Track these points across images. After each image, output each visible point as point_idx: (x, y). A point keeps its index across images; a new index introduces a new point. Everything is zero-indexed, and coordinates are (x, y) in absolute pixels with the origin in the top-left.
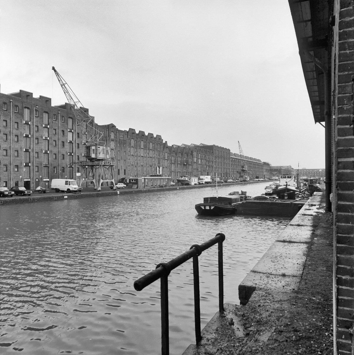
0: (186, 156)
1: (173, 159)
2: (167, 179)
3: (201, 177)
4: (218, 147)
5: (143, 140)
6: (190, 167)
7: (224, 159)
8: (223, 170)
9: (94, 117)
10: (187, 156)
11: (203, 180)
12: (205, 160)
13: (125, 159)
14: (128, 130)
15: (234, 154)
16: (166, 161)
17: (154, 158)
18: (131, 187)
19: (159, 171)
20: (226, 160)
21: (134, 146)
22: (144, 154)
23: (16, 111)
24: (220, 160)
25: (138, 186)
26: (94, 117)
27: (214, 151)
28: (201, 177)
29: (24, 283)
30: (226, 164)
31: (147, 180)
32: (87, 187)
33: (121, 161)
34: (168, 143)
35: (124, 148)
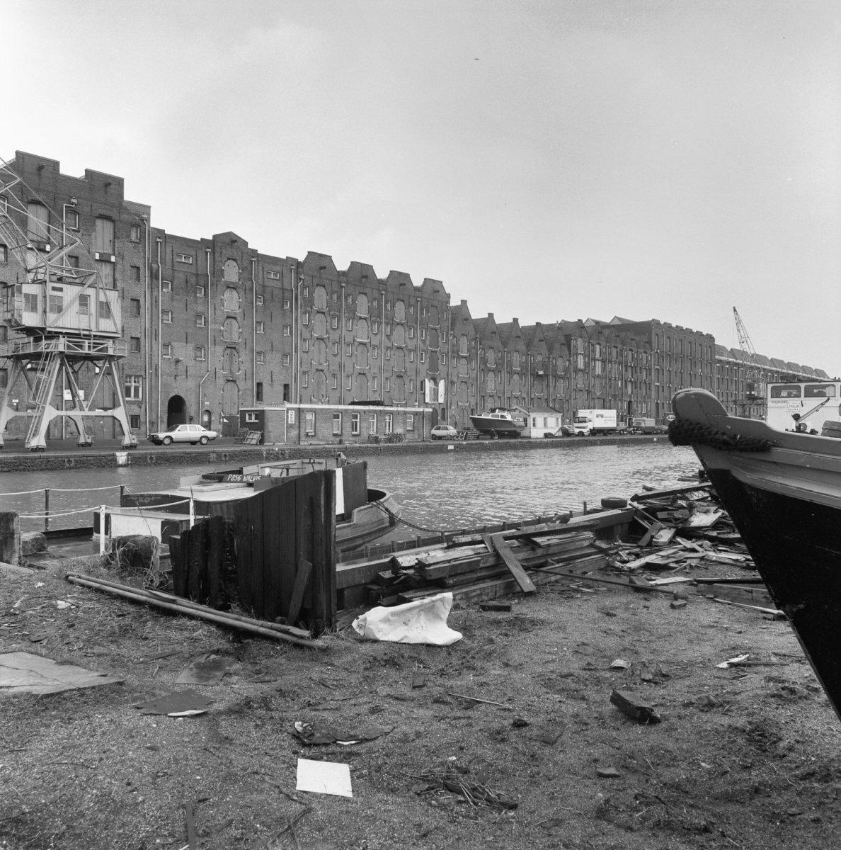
1: (491, 356)
2: (416, 414)
3: (582, 413)
5: (367, 291)
6: (561, 384)
9: (149, 207)
10: (550, 349)
11: (585, 422)
12: (620, 363)
13: (288, 351)
14: (301, 258)
15: (772, 359)
16: (464, 361)
17: (339, 343)
18: (241, 440)
19: (436, 393)
20: (698, 365)
23: (75, 226)
24: (676, 367)
25: (263, 435)
26: (149, 207)
27: (654, 338)
28: (582, 413)
30: (725, 382)
31: (310, 417)
32: (114, 437)
33: (269, 357)
35: (284, 315)
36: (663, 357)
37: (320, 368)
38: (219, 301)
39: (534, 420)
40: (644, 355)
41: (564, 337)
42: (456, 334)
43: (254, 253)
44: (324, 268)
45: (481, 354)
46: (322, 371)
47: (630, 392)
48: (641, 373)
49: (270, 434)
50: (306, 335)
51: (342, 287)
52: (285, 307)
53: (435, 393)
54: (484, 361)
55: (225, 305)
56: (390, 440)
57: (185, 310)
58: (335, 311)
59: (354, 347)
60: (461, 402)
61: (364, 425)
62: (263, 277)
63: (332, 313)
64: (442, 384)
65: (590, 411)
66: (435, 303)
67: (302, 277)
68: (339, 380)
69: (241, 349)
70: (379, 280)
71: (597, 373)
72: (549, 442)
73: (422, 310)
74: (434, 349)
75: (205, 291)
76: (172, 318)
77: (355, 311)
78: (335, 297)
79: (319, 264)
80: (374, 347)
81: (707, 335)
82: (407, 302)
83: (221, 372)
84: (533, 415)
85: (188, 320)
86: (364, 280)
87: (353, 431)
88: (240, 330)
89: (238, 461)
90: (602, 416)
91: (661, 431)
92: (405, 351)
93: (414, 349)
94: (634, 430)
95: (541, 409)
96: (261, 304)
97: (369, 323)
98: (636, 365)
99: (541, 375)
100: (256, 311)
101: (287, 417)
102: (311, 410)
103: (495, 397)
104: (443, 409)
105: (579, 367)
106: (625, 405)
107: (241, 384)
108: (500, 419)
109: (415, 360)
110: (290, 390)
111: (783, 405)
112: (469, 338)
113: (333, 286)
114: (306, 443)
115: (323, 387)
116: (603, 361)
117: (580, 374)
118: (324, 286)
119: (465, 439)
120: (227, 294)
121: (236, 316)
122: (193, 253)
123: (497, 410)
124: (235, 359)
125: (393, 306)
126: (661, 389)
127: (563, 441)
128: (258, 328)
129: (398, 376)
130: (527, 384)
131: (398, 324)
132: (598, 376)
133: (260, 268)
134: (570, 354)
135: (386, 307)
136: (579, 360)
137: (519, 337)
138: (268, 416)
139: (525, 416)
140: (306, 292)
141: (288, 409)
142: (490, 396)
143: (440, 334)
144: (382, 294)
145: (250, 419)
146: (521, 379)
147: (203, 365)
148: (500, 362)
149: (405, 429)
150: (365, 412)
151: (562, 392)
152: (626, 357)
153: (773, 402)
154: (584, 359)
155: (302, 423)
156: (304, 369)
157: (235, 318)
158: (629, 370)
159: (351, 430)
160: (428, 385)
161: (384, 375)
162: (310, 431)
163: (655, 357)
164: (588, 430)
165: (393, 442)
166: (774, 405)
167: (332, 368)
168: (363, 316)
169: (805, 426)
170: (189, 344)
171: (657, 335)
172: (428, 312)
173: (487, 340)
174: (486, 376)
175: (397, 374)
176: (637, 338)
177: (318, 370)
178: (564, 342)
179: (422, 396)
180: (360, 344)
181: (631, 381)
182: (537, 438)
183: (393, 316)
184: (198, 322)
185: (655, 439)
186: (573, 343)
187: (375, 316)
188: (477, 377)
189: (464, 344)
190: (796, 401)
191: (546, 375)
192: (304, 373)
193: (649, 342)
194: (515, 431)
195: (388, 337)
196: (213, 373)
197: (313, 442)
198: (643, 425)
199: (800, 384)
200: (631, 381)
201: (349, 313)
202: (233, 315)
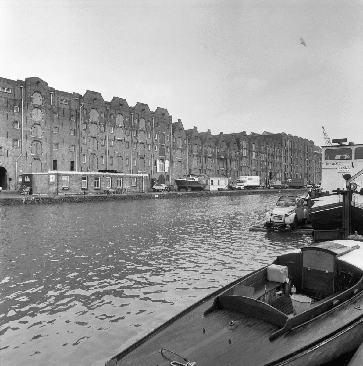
0: (225, 147)
1: (195, 148)
2: (138, 177)
3: (241, 178)
4: (290, 136)
6: (234, 163)
7: (303, 154)
8: (300, 170)
10: (228, 145)
11: (242, 182)
12: (265, 153)
13: (73, 143)
16: (179, 151)
20: (306, 156)
21: (97, 122)
22: (125, 136)
24: (294, 156)
25: (31, 189)
27: (283, 143)
28: (241, 178)
29: (239, 235)
33: (61, 146)
34: (211, 131)
36: (288, 151)
37: (93, 153)
38: (29, 115)
39: (212, 181)
40: (278, 150)
41: (236, 140)
42: (175, 137)
43: (52, 89)
44: (95, 99)
45: (189, 147)
46: (95, 154)
47: (270, 168)
48: (276, 158)
49: (37, 188)
50: (85, 134)
51: (107, 110)
52: (72, 119)
53: (163, 168)
54: (191, 151)
55: (33, 118)
56: (117, 192)
57: (6, 119)
58: (103, 122)
59: (115, 142)
60: (178, 172)
61: (103, 183)
62: (58, 103)
63: (100, 124)
64: (167, 163)
65: (245, 176)
66: (163, 120)
67: (82, 104)
68: (105, 160)
69: (43, 142)
70: (130, 107)
71: (253, 158)
72: (221, 193)
73: (155, 123)
74: (162, 144)
75: (20, 109)
76: (19, 126)
77: (115, 123)
78: (103, 115)
79: (93, 98)
80: (127, 142)
81: (310, 141)
82: (146, 119)
83: (29, 154)
84: (211, 178)
85: (8, 124)
86: (121, 107)
87: (95, 186)
88: (43, 131)
89: (4, 205)
90: (252, 179)
91: (284, 187)
92: (145, 145)
93: (150, 144)
94: (270, 187)
95: (218, 175)
96: (56, 117)
97: (124, 130)
98: (274, 155)
99: (223, 159)
100: (53, 121)
101: (49, 179)
102: (65, 175)
103: (197, 169)
104: (167, 176)
105: (244, 155)
106: (268, 174)
107: (43, 161)
108: (191, 180)
109: (151, 150)
110: (75, 164)
111: (335, 166)
112: (182, 139)
113: (102, 109)
114: (62, 194)
115: (96, 163)
116: (257, 152)
117: (244, 159)
118: (96, 109)
119: (169, 191)
120: (34, 111)
121: (41, 124)
122: (12, 87)
123: (191, 176)
124: (40, 147)
125: (138, 121)
126: (287, 166)
127: (227, 192)
128: (54, 130)
129: (141, 158)
130: (215, 163)
131: (141, 131)
132: (254, 160)
133: (56, 98)
134: (239, 148)
135: (134, 121)
136: (244, 151)
137: (211, 139)
138: (35, 178)
139: (207, 179)
140: (85, 112)
141: (50, 174)
142: (209, 170)
143: (166, 137)
144: (132, 115)
145: (27, 180)
146: (212, 160)
147: (19, 150)
148: (200, 151)
149: (130, 185)
150: (103, 176)
151: (234, 167)
152: (269, 150)
153: (327, 164)
154: (246, 151)
155: (60, 182)
156: (83, 153)
157: (39, 125)
158: (270, 157)
159: (94, 186)
160: (159, 163)
161: (133, 157)
162: (65, 186)
163: (283, 151)
164: (244, 186)
165: (119, 193)
166: (327, 166)
167: (100, 153)
168: (120, 126)
169: (356, 185)
170: (8, 138)
171: (285, 140)
172: (159, 124)
173: (193, 140)
174: (192, 159)
175: (141, 157)
176: (275, 141)
177: (92, 154)
178: (236, 142)
179: (155, 168)
180: (118, 140)
181: (271, 162)
182: (214, 191)
183: (138, 126)
184: (15, 126)
185: (280, 191)
186: (240, 143)
187: (127, 126)
188: (187, 159)
189: (180, 143)
190: (348, 163)
191: (226, 159)
192: (84, 155)
193: (281, 143)
194: (201, 187)
195: (135, 137)
196: (24, 155)
197: (67, 193)
198: (274, 184)
199: (351, 147)
200: (271, 162)
201: (111, 124)
202: (37, 123)
